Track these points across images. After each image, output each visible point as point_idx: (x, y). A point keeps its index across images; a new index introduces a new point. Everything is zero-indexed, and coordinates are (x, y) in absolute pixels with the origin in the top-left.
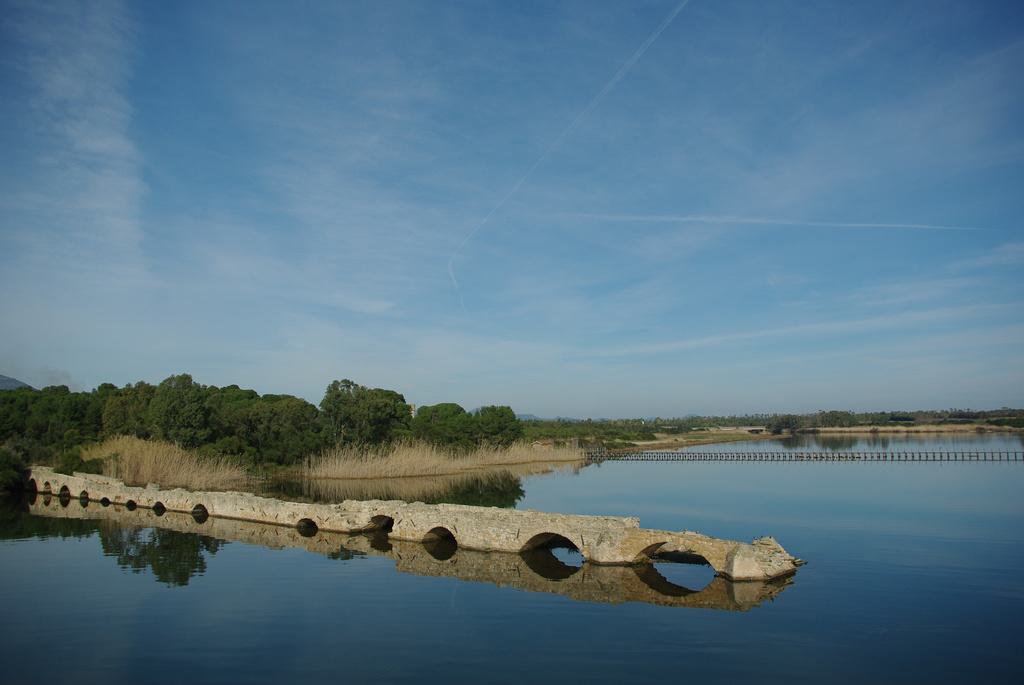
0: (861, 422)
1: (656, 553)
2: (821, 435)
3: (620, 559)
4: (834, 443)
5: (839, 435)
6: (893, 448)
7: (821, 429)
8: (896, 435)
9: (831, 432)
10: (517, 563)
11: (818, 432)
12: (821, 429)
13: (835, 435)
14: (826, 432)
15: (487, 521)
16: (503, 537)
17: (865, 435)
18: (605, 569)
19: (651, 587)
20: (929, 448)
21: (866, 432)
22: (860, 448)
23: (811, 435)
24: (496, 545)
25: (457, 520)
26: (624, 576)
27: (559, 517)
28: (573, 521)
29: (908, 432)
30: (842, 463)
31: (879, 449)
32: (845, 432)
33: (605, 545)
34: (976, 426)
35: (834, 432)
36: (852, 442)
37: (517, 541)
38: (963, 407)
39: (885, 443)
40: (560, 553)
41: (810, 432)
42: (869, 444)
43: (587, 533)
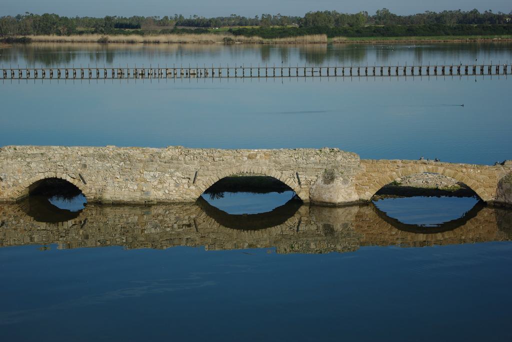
0: (79, 29)
1: (392, 191)
2: (33, 45)
3: (355, 197)
4: (48, 56)
5: (55, 45)
6: (119, 62)
7: (32, 37)
8: (130, 46)
9: (46, 41)
10: (193, 216)
11: (29, 41)
12: (32, 37)
13: (51, 45)
14: (40, 41)
15: (141, 165)
16: (170, 184)
17: (90, 45)
18: (340, 211)
19: (255, 230)
20: (172, 62)
21: (93, 42)
22: (81, 63)
23: (21, 45)
24: (157, 195)
25: (85, 166)
26: (358, 216)
27: (259, 153)
28: (284, 156)
29: (145, 42)
30: (170, 81)
31: (102, 64)
32: (66, 42)
33: (338, 182)
34: (223, 36)
35: (50, 41)
36: (70, 55)
37: (192, 187)
38: (188, 15)
39: (110, 56)
40: (60, 203)
41: (18, 41)
42: (91, 57)
43: (305, 170)
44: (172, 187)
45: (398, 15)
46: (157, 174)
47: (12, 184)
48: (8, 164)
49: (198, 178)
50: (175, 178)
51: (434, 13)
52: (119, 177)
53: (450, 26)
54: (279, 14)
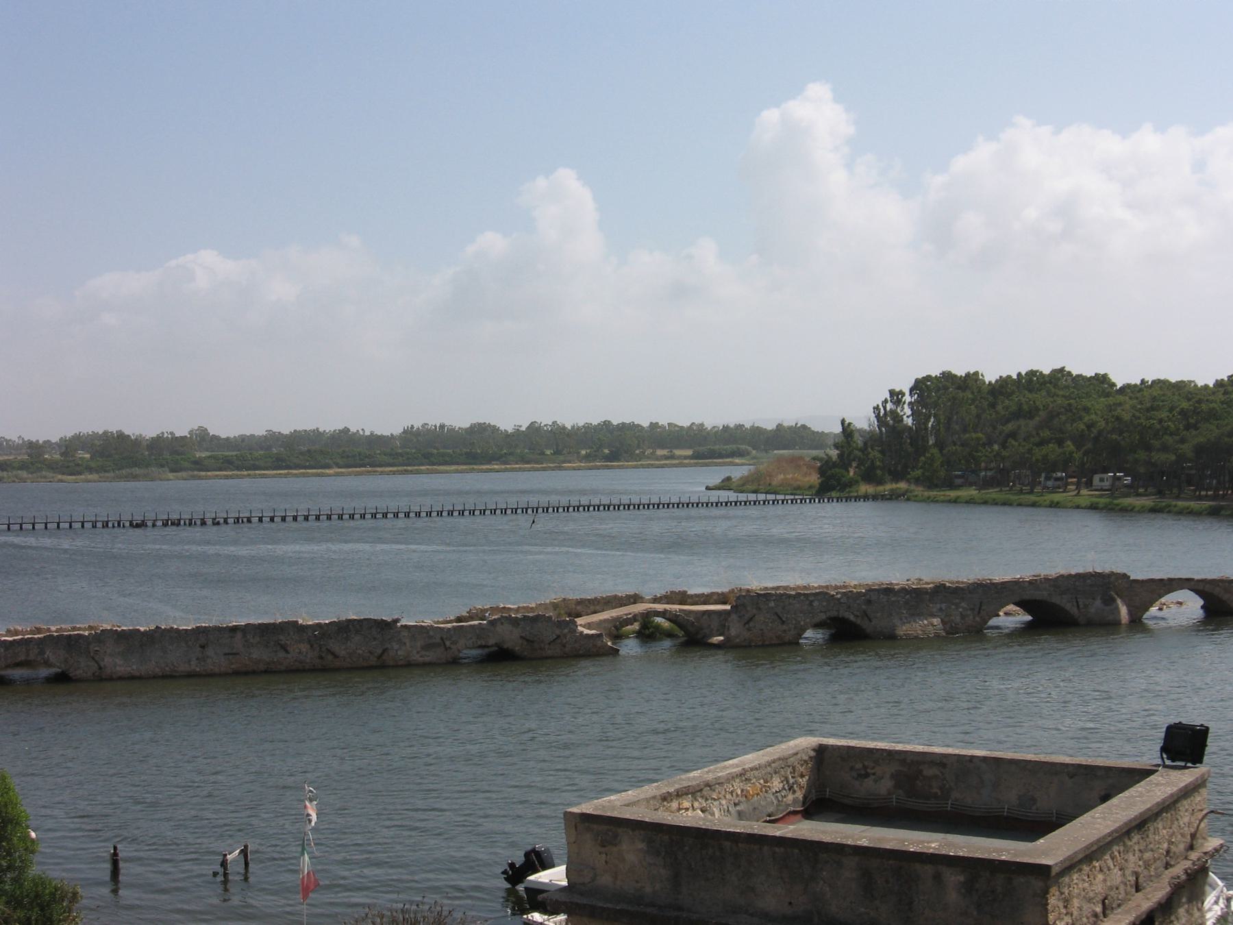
44: (958, 619)
45: (223, 436)
46: (944, 606)
47: (793, 626)
48: (790, 604)
49: (983, 608)
50: (961, 610)
51: (279, 433)
52: (905, 612)
53: (1048, 445)
54: (20, 437)
